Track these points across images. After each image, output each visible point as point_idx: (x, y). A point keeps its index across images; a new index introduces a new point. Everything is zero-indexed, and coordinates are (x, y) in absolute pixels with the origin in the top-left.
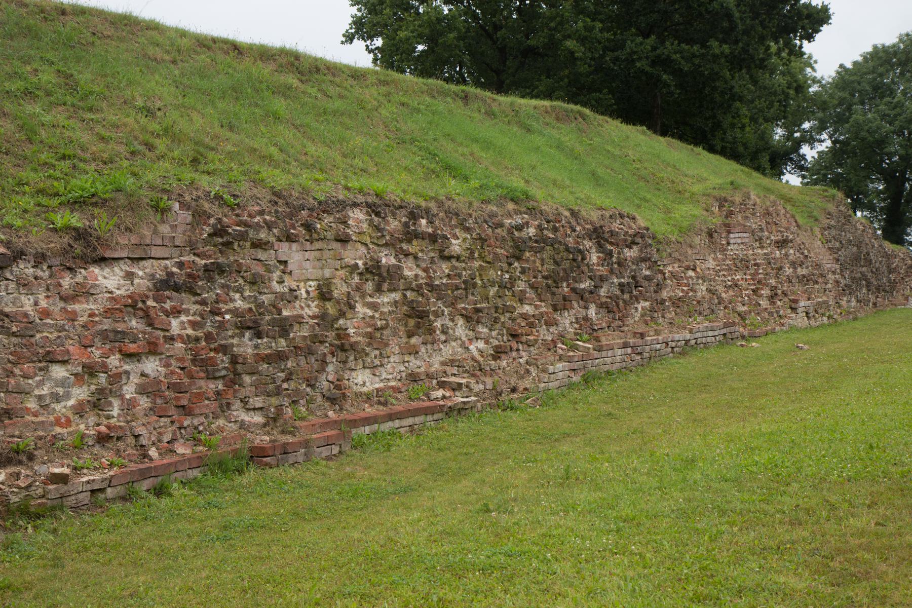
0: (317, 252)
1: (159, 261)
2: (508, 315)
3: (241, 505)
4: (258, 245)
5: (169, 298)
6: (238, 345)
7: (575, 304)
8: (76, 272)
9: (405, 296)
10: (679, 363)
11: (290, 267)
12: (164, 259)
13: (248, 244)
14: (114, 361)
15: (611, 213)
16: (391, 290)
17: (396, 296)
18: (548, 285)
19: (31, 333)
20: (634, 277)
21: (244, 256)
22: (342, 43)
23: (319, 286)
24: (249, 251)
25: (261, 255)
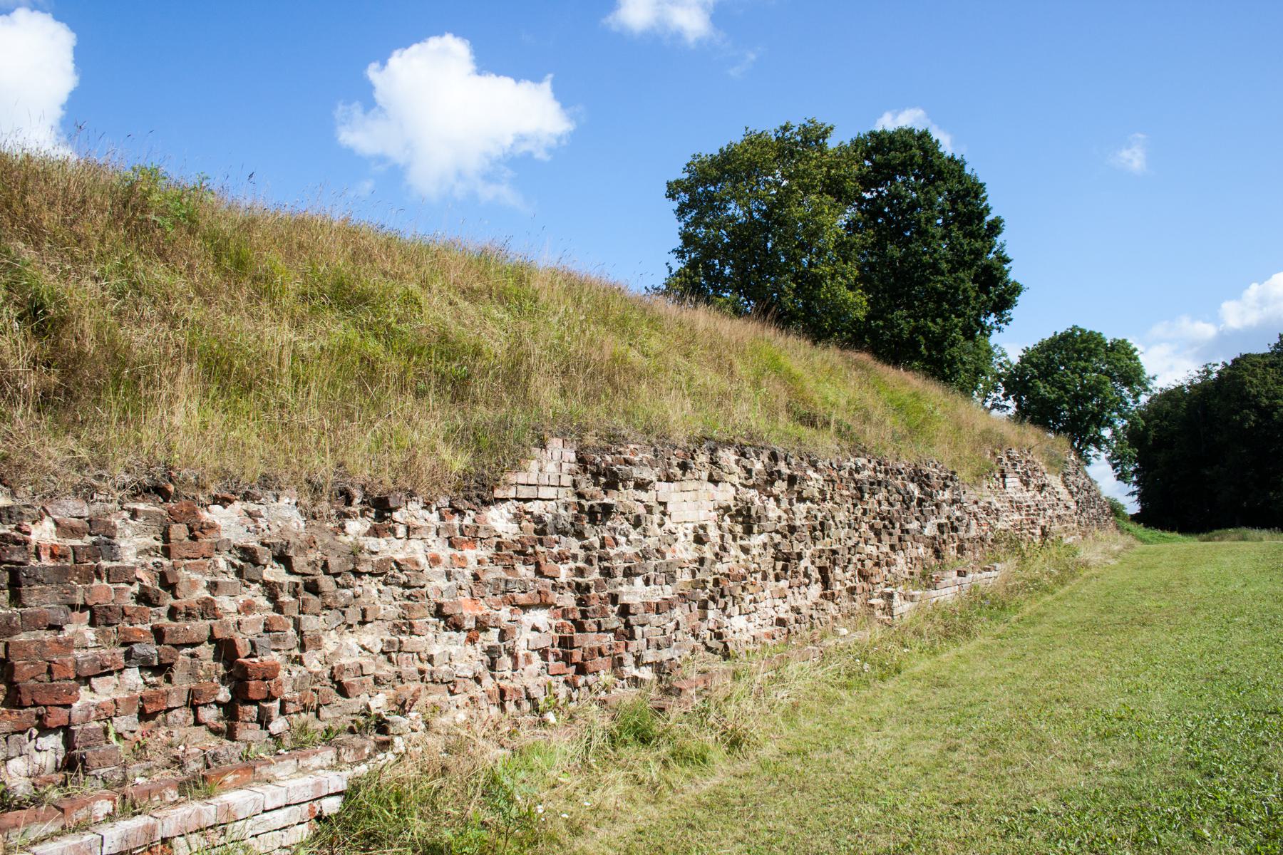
0: (692, 493)
1: (546, 502)
2: (858, 556)
3: (908, 698)
4: (642, 486)
5: (557, 542)
6: (628, 593)
8: (465, 514)
9: (772, 538)
10: (912, 598)
11: (670, 509)
12: (549, 500)
13: (631, 484)
14: (505, 613)
15: (543, 298)
16: (760, 533)
17: (764, 538)
18: (885, 527)
19: (422, 583)
20: (949, 518)
21: (624, 498)
22: (469, 75)
23: (695, 527)
24: (632, 492)
25: (642, 495)
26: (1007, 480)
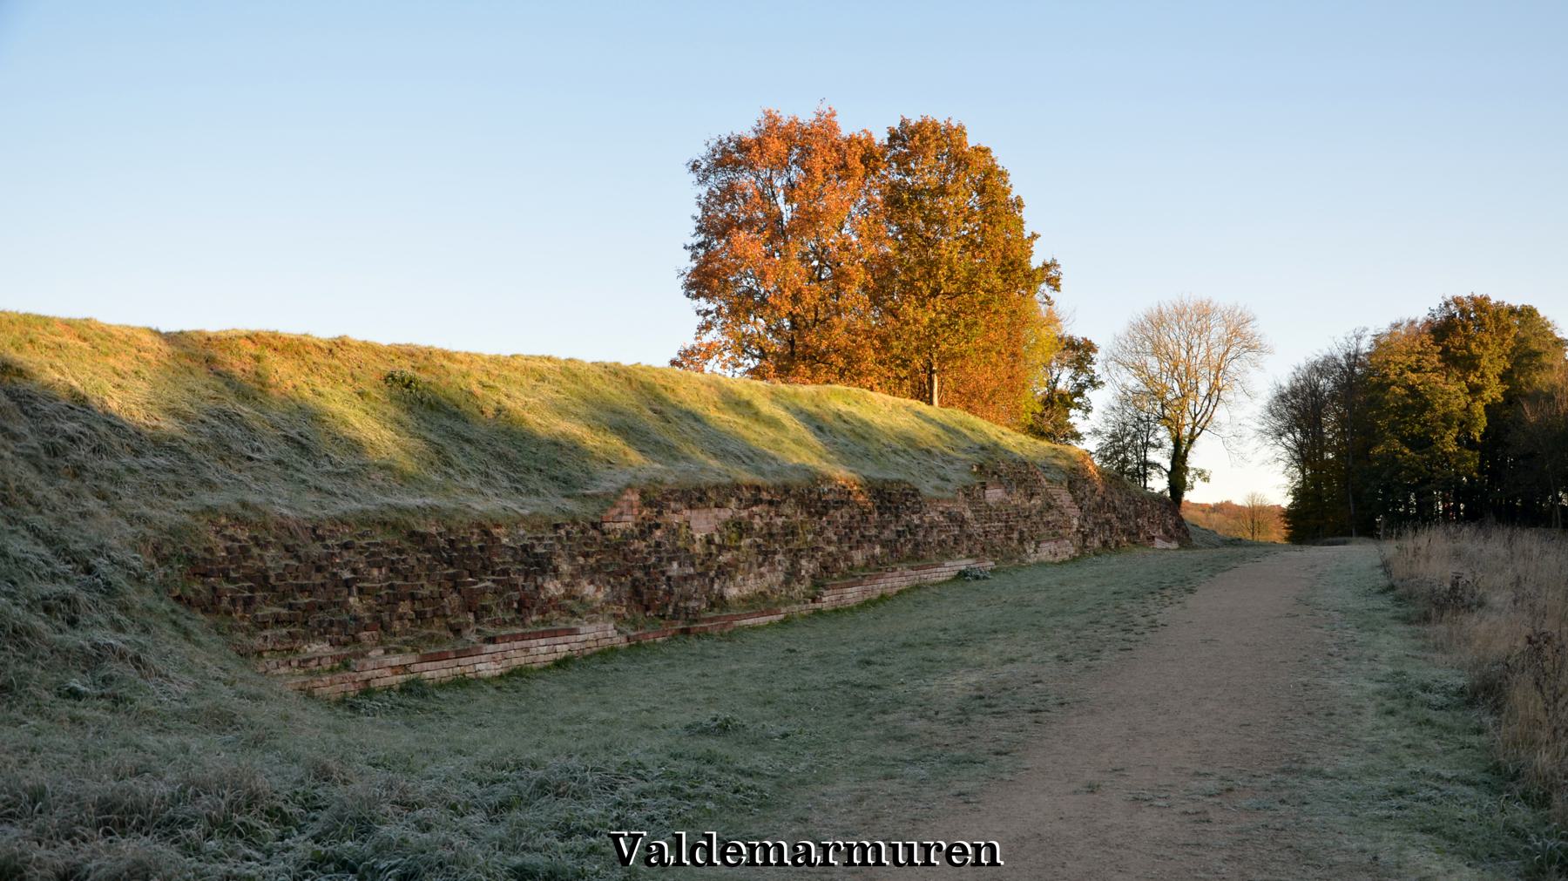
7: (865, 545)
26: (987, 492)
